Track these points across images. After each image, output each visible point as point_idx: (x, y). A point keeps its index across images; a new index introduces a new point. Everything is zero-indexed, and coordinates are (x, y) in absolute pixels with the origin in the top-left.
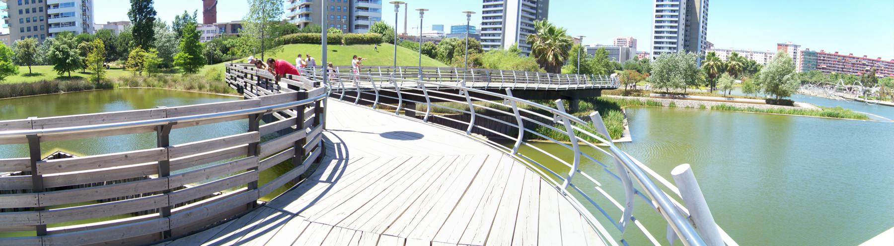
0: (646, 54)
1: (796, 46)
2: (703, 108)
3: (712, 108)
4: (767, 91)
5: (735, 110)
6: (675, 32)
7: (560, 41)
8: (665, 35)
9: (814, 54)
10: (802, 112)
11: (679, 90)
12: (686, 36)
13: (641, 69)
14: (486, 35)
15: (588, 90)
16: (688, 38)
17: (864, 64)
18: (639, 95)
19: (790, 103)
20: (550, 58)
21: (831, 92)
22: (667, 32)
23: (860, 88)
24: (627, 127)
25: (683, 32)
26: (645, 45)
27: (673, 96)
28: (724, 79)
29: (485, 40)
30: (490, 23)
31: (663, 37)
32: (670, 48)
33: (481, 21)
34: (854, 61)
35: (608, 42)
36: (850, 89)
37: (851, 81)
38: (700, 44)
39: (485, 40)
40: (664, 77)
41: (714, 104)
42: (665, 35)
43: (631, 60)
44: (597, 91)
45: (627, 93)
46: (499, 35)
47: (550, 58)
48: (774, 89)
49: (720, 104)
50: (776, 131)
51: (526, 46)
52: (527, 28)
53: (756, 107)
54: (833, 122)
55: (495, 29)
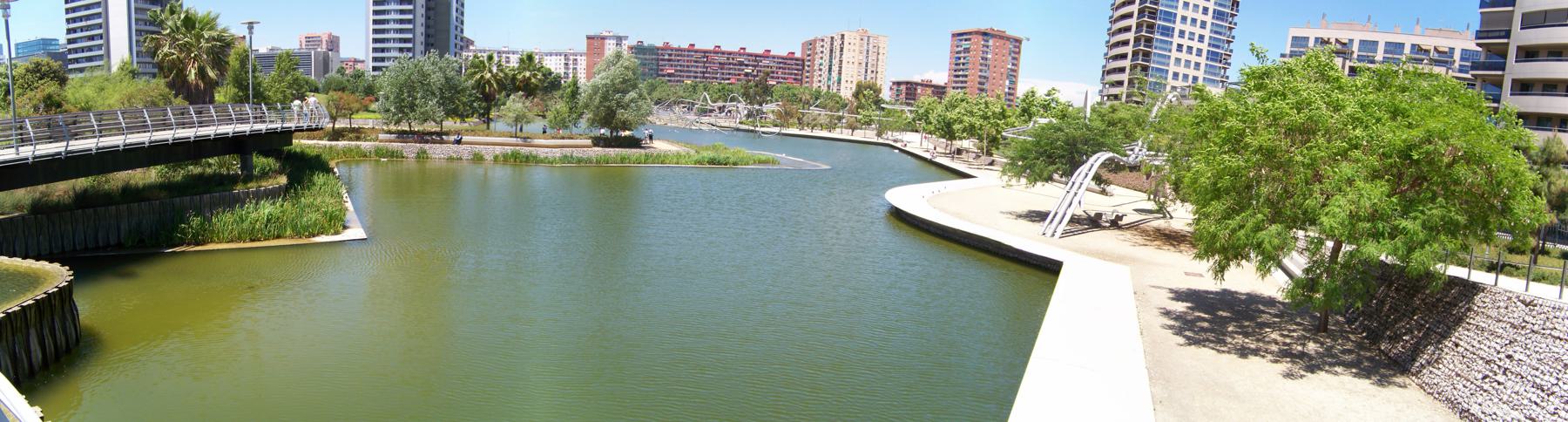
0: (356, 61)
1: (619, 39)
2: (478, 159)
3: (496, 158)
4: (593, 123)
5: (537, 160)
6: (409, 21)
7: (208, 41)
8: (392, 26)
9: (653, 50)
10: (661, 158)
11: (431, 126)
12: (427, 27)
13: (352, 89)
14: (76, 51)
15: (272, 134)
16: (432, 31)
17: (741, 64)
18: (358, 139)
19: (634, 143)
20: (192, 75)
21: (692, 117)
22: (396, 21)
23: (743, 107)
24: (349, 205)
25: (423, 20)
26: (356, 46)
27: (422, 137)
28: (515, 104)
29: (77, 61)
30: (82, 29)
31: (388, 31)
32: (401, 50)
33: (65, 27)
34: (723, 59)
35: (290, 42)
36: (721, 109)
37: (725, 95)
38: (452, 41)
39: (77, 61)
40: (404, 105)
41: (498, 150)
42: (392, 26)
43: (333, 74)
44: (287, 135)
45: (337, 135)
46: (99, 47)
47: (192, 75)
48: (608, 119)
49: (509, 149)
50: (612, 197)
51: (148, 59)
52: (145, 28)
53: (577, 153)
54: (720, 172)
55: (92, 38)
